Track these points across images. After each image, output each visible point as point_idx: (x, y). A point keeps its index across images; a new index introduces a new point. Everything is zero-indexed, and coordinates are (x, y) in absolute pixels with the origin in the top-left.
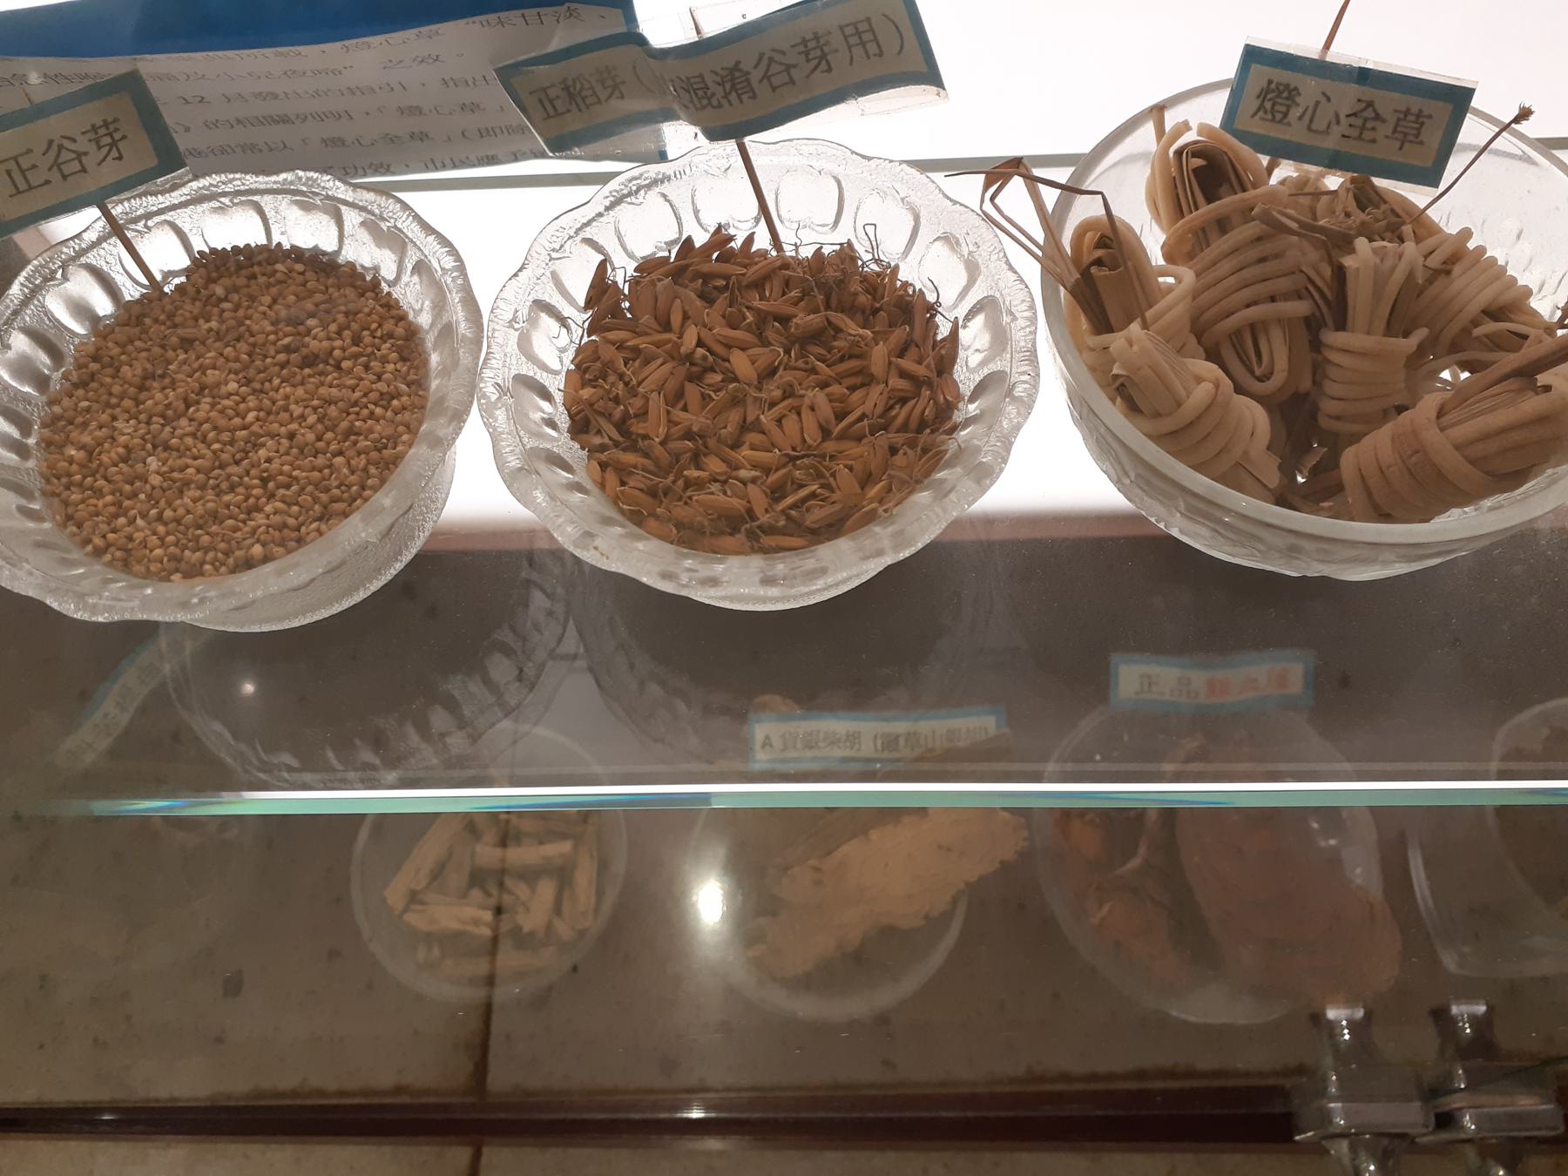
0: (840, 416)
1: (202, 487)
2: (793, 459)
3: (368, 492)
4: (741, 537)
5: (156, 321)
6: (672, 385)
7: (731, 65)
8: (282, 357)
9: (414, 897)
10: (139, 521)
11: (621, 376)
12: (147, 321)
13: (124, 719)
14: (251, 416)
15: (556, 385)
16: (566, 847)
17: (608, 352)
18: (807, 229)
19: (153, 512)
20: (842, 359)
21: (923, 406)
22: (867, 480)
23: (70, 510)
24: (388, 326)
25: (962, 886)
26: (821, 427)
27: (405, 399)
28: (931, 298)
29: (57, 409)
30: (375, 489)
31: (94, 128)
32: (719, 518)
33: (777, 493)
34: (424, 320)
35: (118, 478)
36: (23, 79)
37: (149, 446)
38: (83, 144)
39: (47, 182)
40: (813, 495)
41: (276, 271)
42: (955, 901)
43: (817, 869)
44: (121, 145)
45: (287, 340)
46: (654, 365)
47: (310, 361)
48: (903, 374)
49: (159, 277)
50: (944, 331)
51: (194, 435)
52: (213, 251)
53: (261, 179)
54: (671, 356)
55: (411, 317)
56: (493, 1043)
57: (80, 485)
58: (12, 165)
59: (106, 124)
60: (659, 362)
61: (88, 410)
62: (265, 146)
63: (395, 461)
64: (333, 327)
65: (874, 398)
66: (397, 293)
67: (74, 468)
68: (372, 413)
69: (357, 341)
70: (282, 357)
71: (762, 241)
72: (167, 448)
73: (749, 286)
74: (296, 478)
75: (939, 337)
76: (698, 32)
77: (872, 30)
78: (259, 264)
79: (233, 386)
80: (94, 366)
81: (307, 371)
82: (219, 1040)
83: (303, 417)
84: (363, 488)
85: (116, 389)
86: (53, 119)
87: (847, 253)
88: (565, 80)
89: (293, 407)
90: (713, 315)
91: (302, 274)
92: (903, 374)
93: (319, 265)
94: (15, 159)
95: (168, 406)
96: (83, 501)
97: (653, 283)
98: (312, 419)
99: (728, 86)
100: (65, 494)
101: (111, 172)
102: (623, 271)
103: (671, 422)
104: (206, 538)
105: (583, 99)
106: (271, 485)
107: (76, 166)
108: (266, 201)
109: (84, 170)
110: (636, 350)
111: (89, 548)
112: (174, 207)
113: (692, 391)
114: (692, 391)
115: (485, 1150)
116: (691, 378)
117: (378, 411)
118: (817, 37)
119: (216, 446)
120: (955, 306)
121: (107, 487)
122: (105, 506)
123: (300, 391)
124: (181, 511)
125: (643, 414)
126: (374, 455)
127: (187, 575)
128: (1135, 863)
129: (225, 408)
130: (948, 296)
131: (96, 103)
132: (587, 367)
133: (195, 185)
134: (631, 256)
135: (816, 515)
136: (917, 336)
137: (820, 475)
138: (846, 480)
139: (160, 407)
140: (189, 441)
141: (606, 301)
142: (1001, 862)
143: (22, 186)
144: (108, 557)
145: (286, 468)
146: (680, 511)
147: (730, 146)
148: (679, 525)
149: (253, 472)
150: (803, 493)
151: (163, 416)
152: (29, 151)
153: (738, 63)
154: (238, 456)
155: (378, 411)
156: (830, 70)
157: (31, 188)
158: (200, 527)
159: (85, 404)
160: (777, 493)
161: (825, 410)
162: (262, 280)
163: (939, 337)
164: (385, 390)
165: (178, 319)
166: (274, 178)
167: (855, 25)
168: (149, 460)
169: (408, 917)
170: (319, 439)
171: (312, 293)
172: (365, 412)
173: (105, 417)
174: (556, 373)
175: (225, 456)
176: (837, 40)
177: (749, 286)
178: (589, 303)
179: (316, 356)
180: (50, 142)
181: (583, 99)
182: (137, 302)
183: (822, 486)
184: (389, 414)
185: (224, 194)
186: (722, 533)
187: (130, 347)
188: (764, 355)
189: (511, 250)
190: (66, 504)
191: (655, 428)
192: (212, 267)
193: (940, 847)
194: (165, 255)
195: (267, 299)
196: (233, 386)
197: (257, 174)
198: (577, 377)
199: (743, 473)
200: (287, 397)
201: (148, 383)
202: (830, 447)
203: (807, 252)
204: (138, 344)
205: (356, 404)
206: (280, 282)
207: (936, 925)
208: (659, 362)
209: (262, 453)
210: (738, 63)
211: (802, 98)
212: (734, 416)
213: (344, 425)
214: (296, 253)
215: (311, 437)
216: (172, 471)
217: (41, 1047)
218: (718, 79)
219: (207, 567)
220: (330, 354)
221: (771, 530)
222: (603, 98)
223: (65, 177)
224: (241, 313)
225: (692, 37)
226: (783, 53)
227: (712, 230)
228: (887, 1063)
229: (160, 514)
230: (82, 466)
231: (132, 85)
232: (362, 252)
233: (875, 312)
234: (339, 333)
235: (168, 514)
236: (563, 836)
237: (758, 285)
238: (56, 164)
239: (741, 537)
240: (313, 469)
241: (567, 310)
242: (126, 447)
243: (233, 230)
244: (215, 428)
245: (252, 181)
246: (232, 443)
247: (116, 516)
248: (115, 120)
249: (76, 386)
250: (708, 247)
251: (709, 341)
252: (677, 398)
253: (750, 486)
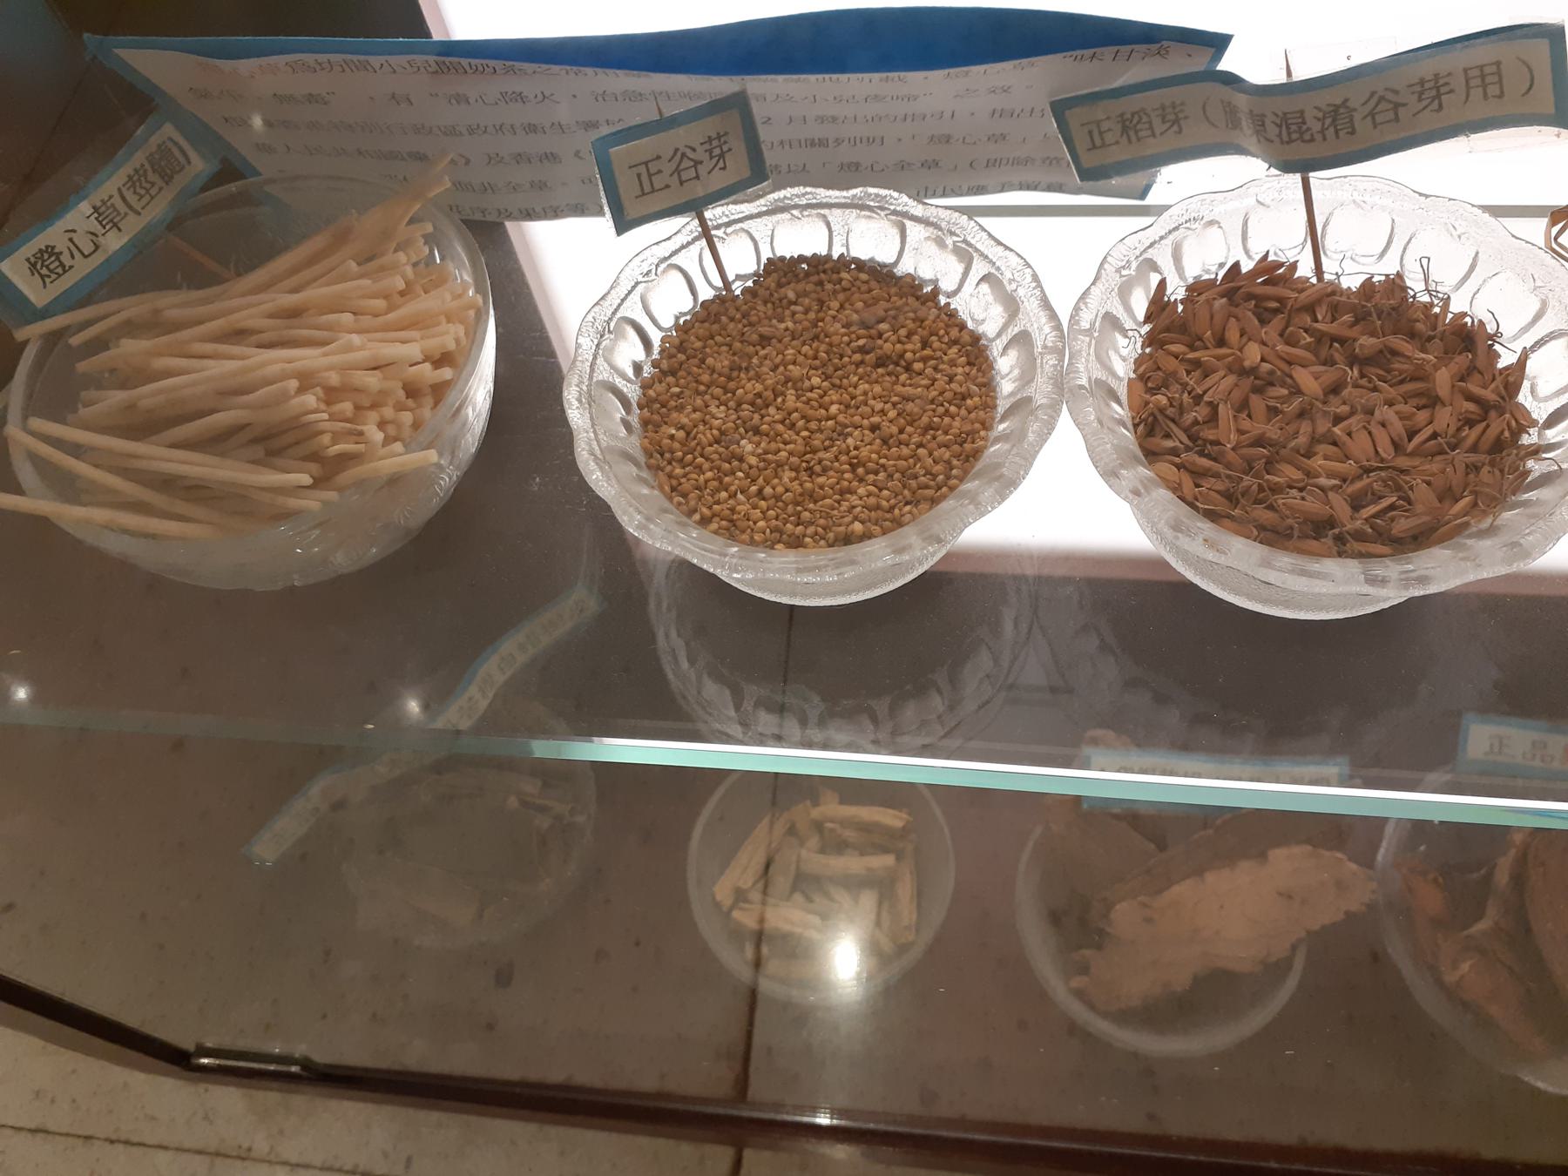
0: (1411, 435)
1: (796, 469)
2: (1368, 471)
3: (953, 482)
4: (1329, 541)
5: (732, 319)
6: (1237, 395)
7: (1338, 101)
8: (857, 357)
9: (740, 896)
10: (739, 496)
11: (1184, 385)
12: (724, 318)
13: (483, 704)
14: (834, 409)
15: (1122, 392)
16: (889, 860)
17: (1171, 364)
18: (1352, 262)
19: (754, 488)
20: (1402, 382)
21: (1496, 425)
22: (1448, 495)
23: (674, 482)
24: (954, 333)
25: (1303, 934)
26: (1393, 442)
27: (976, 399)
28: (1491, 328)
29: (651, 393)
30: (961, 480)
31: (710, 140)
32: (1305, 521)
33: (1356, 504)
34: (989, 328)
35: (715, 456)
36: (268, 123)
37: (742, 430)
38: (701, 154)
39: (667, 186)
40: (1392, 507)
41: (841, 279)
42: (1294, 948)
43: (1144, 905)
44: (727, 156)
45: (861, 342)
46: (1215, 377)
47: (881, 362)
48: (1470, 397)
49: (731, 277)
50: (1506, 359)
51: (782, 422)
52: (782, 259)
53: (831, 193)
54: (1230, 370)
55: (970, 325)
56: (754, 1054)
57: (681, 460)
58: (642, 169)
59: (719, 137)
60: (1222, 373)
61: (678, 396)
62: (845, 166)
63: (976, 454)
64: (903, 332)
65: (1445, 418)
66: (955, 303)
67: (676, 445)
68: (947, 411)
69: (925, 344)
70: (857, 357)
71: (1305, 270)
72: (757, 431)
73: (1300, 310)
74: (883, 466)
75: (1500, 365)
76: (1289, 73)
77: (1499, 73)
78: (824, 272)
79: (816, 381)
80: (681, 357)
81: (880, 370)
82: (490, 1027)
83: (883, 412)
84: (948, 478)
85: (705, 378)
86: (681, 131)
87: (1395, 284)
88: (1122, 115)
89: (871, 402)
90: (1270, 332)
91: (866, 282)
92: (1470, 397)
93: (879, 275)
94: (646, 163)
95: (759, 395)
96: (685, 476)
97: (1209, 302)
98: (892, 414)
99: (1328, 121)
100: (669, 468)
101: (718, 181)
102: (1176, 291)
103: (1241, 432)
104: (806, 515)
105: (1136, 132)
106: (860, 470)
107: (692, 173)
108: (835, 216)
109: (697, 177)
110: (1197, 364)
111: (697, 517)
112: (830, 206)
113: (1255, 400)
114: (1255, 400)
115: (748, 1154)
116: (1258, 390)
117: (953, 409)
118: (1437, 77)
119: (805, 433)
120: (1515, 338)
121: (706, 466)
122: (706, 482)
123: (877, 389)
124: (780, 489)
125: (1213, 418)
126: (956, 448)
127: (789, 546)
128: (1482, 926)
129: (810, 400)
130: (1508, 330)
131: (710, 119)
132: (1149, 376)
133: (775, 195)
134: (1181, 275)
135: (1402, 525)
136: (1480, 363)
137: (1399, 488)
138: (1423, 494)
139: (750, 396)
140: (780, 427)
141: (1164, 320)
142: (1347, 913)
143: (647, 188)
144: (714, 526)
145: (874, 456)
146: (1266, 516)
147: (1296, 178)
148: (1262, 528)
149: (844, 458)
150: (1385, 503)
151: (752, 404)
152: (659, 157)
153: (1346, 100)
154: (827, 443)
155: (953, 409)
156: (1180, 132)
157: (653, 191)
158: (798, 504)
159: (677, 390)
160: (1356, 504)
161: (1398, 427)
162: (829, 286)
163: (1500, 365)
164: (959, 390)
165: (754, 319)
166: (845, 193)
167: (1481, 67)
168: (743, 442)
169: (736, 914)
170: (901, 431)
171: (876, 300)
172: (941, 410)
173: (699, 402)
174: (1120, 379)
175: (816, 443)
176: (1458, 83)
177: (1300, 310)
178: (1148, 319)
179: (888, 357)
180: (677, 150)
181: (1136, 132)
182: (712, 301)
183: (1400, 498)
184: (963, 412)
185: (796, 207)
186: (1307, 537)
187: (711, 342)
188: (1330, 375)
189: (1055, 270)
190: (670, 476)
191: (1227, 432)
192: (780, 270)
193: (1280, 894)
194: (741, 260)
195: (835, 305)
196: (816, 381)
197: (828, 188)
198: (1140, 386)
199: (1323, 481)
200: (865, 393)
201: (735, 374)
202: (1403, 462)
203: (1352, 282)
204: (718, 338)
205: (932, 402)
206: (845, 290)
208: (1222, 373)
209: (850, 441)
210: (1346, 100)
211: (1402, 135)
212: (1305, 427)
213: (925, 419)
214: (861, 265)
215: (894, 429)
216: (766, 453)
217: (324, 1017)
218: (1320, 115)
219: (808, 540)
220: (902, 356)
221: (1359, 536)
222: (1158, 132)
223: (681, 183)
224: (812, 315)
225: (1281, 78)
226: (1396, 92)
227: (1257, 257)
228: (1151, 1117)
229: (760, 491)
230: (683, 444)
231: (739, 103)
232: (927, 262)
233: (1430, 339)
234: (908, 336)
235: (768, 490)
236: (885, 850)
237: (1310, 308)
238: (678, 171)
239: (1329, 541)
240: (899, 458)
241: (1129, 324)
242: (719, 429)
243: (800, 238)
244: (803, 417)
245: (823, 194)
246: (820, 430)
247: (718, 491)
248: (726, 134)
249: (664, 373)
250: (1254, 273)
251: (1271, 357)
252: (1243, 406)
253: (1331, 494)
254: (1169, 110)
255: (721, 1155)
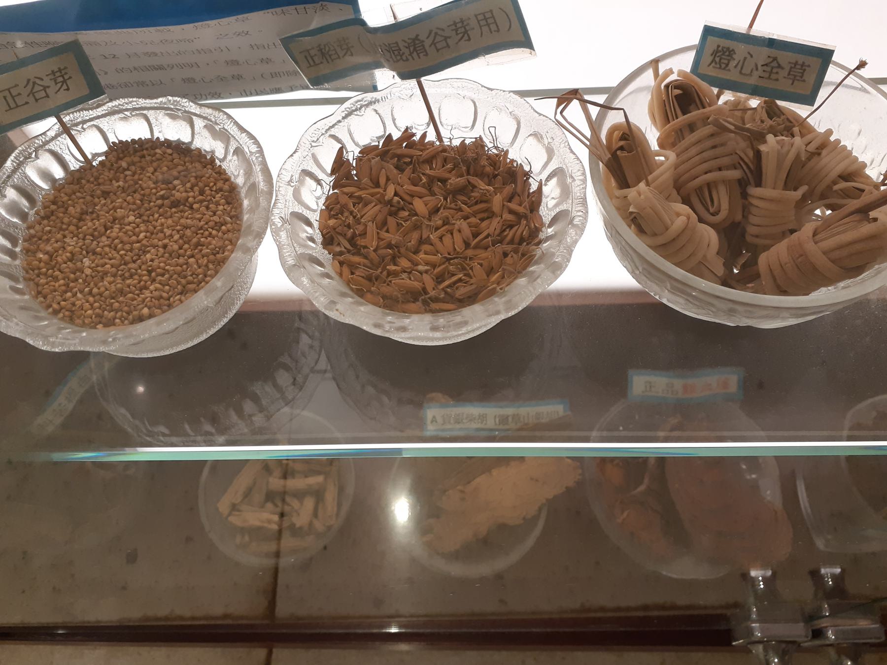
0: (475, 235)
1: (115, 276)
2: (449, 260)
3: (208, 278)
4: (419, 304)
5: (88, 181)
6: (380, 218)
7: (413, 37)
8: (159, 202)
9: (234, 508)
10: (79, 295)
11: (351, 213)
12: (83, 181)
13: (70, 407)
14: (142, 235)
15: (314, 217)
16: (320, 479)
17: (344, 199)
18: (457, 129)
19: (87, 289)
20: (476, 203)
21: (522, 229)
22: (490, 271)
23: (40, 288)
24: (220, 184)
25: (544, 501)
26: (465, 242)
27: (229, 225)
28: (527, 168)
29: (32, 231)
30: (212, 277)
31: (53, 73)
32: (407, 293)
33: (439, 279)
34: (240, 181)
35: (67, 270)
36: (13, 45)
37: (84, 252)
38: (47, 82)
39: (27, 103)
40: (460, 280)
41: (156, 153)
42: (540, 510)
43: (462, 492)
44: (68, 82)
45: (162, 193)
46: (370, 206)
47: (175, 204)
48: (511, 212)
49: (90, 157)
50: (534, 187)
51: (110, 246)
52: (121, 142)
53: (148, 101)
54: (380, 202)
55: (232, 179)
56: (279, 590)
57: (45, 274)
58: (7, 93)
59: (60, 70)
60: (373, 204)
61: (50, 232)
62: (150, 82)
63: (224, 261)
64: (188, 185)
65: (494, 225)
66: (224, 166)
67: (42, 264)
68: (210, 234)
69: (202, 193)
70: (159, 202)
71: (431, 137)
72: (94, 253)
73: (424, 162)
74: (167, 270)
75: (531, 191)
76: (395, 18)
77: (493, 17)
78: (147, 149)
79: (132, 218)
80: (53, 207)
81: (174, 210)
82: (124, 588)
83: (171, 236)
84: (205, 276)
85: (66, 220)
86: (30, 67)
87: (479, 143)
88: (320, 45)
89: (166, 230)
90: (403, 178)
91: (171, 155)
92: (511, 212)
93: (181, 150)
94: (9, 90)
95: (95, 230)
96: (47, 283)
97: (369, 160)
98: (176, 237)
99: (412, 49)
100: (37, 279)
101: (63, 97)
102: (352, 153)
103: (380, 239)
104: (117, 304)
105: (330, 56)
106: (153, 274)
107: (43, 94)
108: (151, 114)
109: (47, 96)
110: (360, 198)
111: (51, 310)
112: (98, 117)
113: (391, 221)
114: (391, 221)
115: (274, 650)
116: (391, 214)
117: (214, 232)
118: (462, 21)
119: (122, 252)
120: (540, 173)
121: (60, 276)
122: (60, 286)
123: (170, 221)
124: (102, 289)
125: (364, 234)
126: (212, 257)
127: (106, 325)
128: (642, 488)
129: (127, 231)
130: (536, 168)
131: (54, 58)
132: (332, 208)
133: (110, 104)
134: (357, 144)
135: (462, 291)
136: (519, 190)
137: (464, 269)
138: (478, 272)
139: (91, 230)
140: (107, 249)
141: (343, 170)
142: (566, 488)
143: (13, 105)
144: (61, 315)
145: (162, 265)
146: (385, 289)
147: (413, 82)
148: (384, 297)
149: (143, 267)
150: (454, 279)
151: (92, 235)
152: (16, 86)
153: (417, 35)
154: (134, 258)
155: (214, 232)
156: (469, 39)
157: (17, 106)
158: (113, 298)
159: (48, 228)
160: (439, 279)
161: (467, 232)
162: (148, 158)
163: (531, 191)
164: (218, 220)
165: (101, 181)
166: (155, 101)
167: (484, 14)
168: (85, 260)
169: (231, 519)
170: (181, 248)
171: (176, 166)
172: (207, 233)
173: (59, 236)
174: (314, 211)
175: (127, 258)
176: (473, 23)
177: (424, 162)
178: (333, 171)
179: (179, 201)
180: (29, 81)
181: (330, 56)
182: (78, 171)
183: (465, 275)
184: (220, 234)
185: (127, 110)
186: (409, 301)
187: (74, 196)
188: (432, 201)
189: (289, 142)
190: (37, 285)
191: (371, 242)
192: (120, 151)
193: (532, 479)
194: (94, 144)
195: (151, 169)
196: (132, 218)
197: (145, 98)
198: (326, 213)
199: (420, 268)
200: (162, 225)
201: (84, 217)
202: (470, 253)
203: (456, 143)
204: (78, 194)
205: (201, 228)
206: (158, 160)
207: (529, 523)
208: (373, 204)
209: (148, 256)
210: (417, 35)
211: (454, 55)
212: (415, 235)
213: (195, 240)
214: (168, 143)
215: (176, 247)
216: (97, 266)
217: (23, 592)
218: (406, 45)
219: (117, 321)
220: (187, 200)
221: (436, 300)
222: (341, 55)
223: (37, 100)
224: (136, 177)
225: (391, 21)
226: (443, 30)
227: (403, 130)
228: (502, 601)
229: (91, 291)
230: (46, 263)
231: (75, 48)
232: (205, 142)
233: (495, 176)
234: (192, 188)
235: (95, 290)
236: (319, 473)
237: (429, 161)
238: (32, 93)
239: (419, 304)
240: (177, 265)
241: (321, 176)
242: (71, 253)
243: (132, 130)
244: (122, 242)
245: (143, 102)
246: (131, 250)
247: (66, 292)
248: (65, 68)
249: (43, 218)
250: (401, 140)
251: (401, 193)
252: (383, 225)
253: (424, 275)
254: (459, 25)
255: (260, 653)
